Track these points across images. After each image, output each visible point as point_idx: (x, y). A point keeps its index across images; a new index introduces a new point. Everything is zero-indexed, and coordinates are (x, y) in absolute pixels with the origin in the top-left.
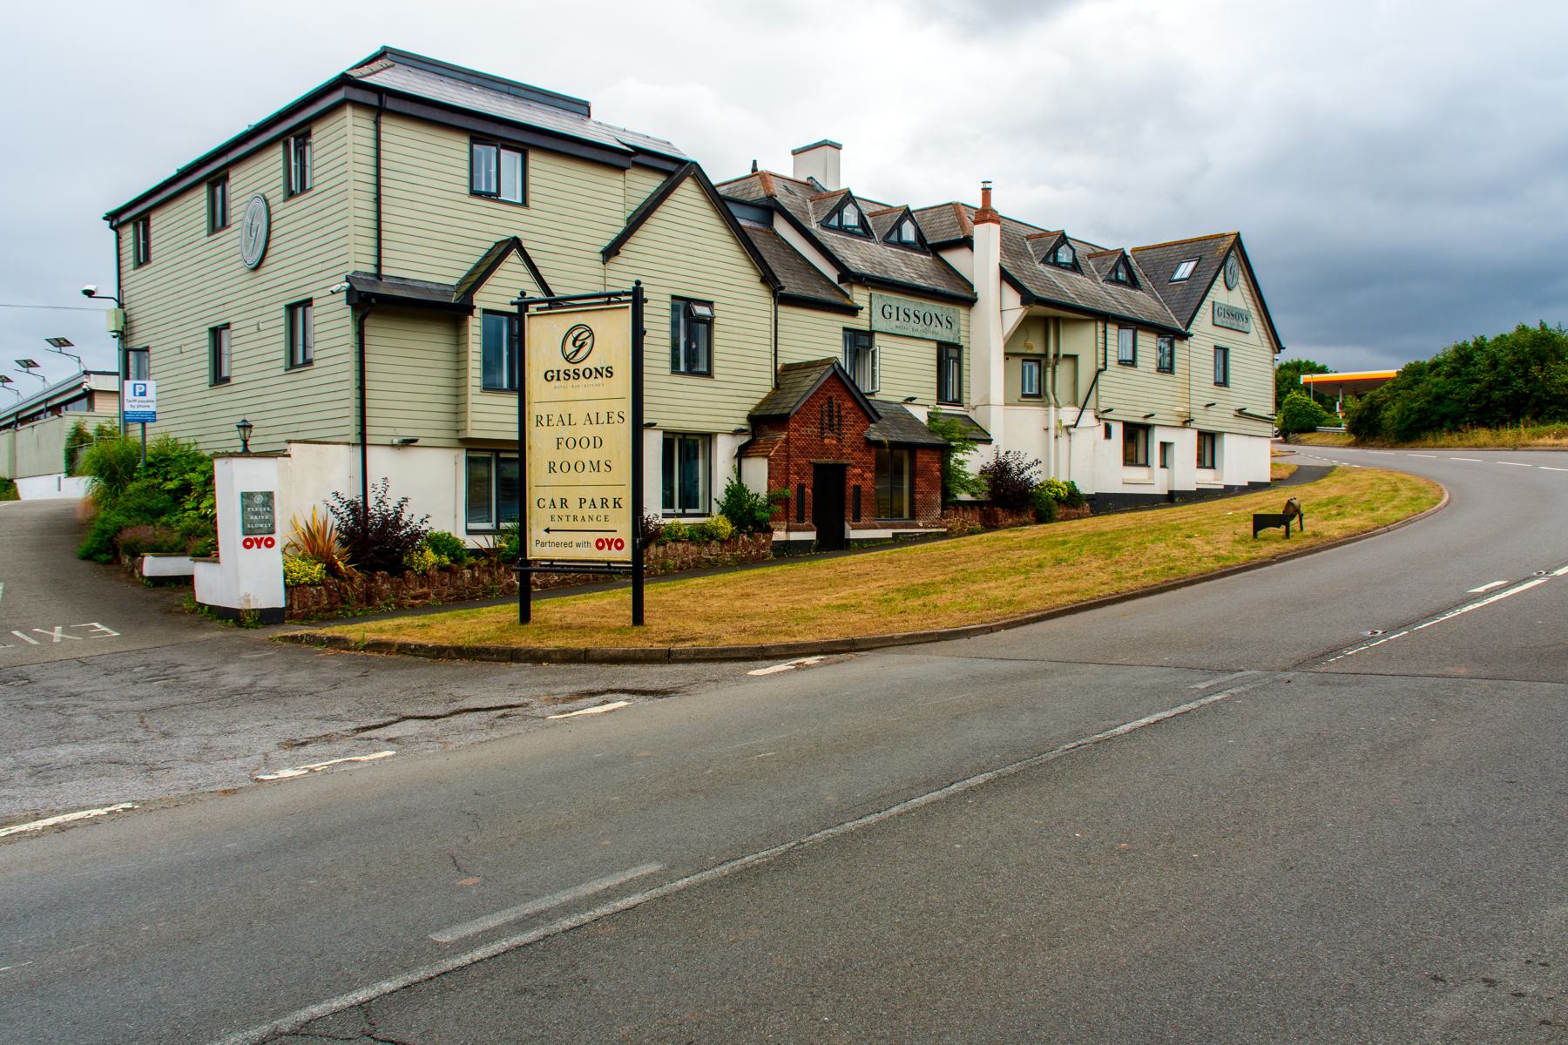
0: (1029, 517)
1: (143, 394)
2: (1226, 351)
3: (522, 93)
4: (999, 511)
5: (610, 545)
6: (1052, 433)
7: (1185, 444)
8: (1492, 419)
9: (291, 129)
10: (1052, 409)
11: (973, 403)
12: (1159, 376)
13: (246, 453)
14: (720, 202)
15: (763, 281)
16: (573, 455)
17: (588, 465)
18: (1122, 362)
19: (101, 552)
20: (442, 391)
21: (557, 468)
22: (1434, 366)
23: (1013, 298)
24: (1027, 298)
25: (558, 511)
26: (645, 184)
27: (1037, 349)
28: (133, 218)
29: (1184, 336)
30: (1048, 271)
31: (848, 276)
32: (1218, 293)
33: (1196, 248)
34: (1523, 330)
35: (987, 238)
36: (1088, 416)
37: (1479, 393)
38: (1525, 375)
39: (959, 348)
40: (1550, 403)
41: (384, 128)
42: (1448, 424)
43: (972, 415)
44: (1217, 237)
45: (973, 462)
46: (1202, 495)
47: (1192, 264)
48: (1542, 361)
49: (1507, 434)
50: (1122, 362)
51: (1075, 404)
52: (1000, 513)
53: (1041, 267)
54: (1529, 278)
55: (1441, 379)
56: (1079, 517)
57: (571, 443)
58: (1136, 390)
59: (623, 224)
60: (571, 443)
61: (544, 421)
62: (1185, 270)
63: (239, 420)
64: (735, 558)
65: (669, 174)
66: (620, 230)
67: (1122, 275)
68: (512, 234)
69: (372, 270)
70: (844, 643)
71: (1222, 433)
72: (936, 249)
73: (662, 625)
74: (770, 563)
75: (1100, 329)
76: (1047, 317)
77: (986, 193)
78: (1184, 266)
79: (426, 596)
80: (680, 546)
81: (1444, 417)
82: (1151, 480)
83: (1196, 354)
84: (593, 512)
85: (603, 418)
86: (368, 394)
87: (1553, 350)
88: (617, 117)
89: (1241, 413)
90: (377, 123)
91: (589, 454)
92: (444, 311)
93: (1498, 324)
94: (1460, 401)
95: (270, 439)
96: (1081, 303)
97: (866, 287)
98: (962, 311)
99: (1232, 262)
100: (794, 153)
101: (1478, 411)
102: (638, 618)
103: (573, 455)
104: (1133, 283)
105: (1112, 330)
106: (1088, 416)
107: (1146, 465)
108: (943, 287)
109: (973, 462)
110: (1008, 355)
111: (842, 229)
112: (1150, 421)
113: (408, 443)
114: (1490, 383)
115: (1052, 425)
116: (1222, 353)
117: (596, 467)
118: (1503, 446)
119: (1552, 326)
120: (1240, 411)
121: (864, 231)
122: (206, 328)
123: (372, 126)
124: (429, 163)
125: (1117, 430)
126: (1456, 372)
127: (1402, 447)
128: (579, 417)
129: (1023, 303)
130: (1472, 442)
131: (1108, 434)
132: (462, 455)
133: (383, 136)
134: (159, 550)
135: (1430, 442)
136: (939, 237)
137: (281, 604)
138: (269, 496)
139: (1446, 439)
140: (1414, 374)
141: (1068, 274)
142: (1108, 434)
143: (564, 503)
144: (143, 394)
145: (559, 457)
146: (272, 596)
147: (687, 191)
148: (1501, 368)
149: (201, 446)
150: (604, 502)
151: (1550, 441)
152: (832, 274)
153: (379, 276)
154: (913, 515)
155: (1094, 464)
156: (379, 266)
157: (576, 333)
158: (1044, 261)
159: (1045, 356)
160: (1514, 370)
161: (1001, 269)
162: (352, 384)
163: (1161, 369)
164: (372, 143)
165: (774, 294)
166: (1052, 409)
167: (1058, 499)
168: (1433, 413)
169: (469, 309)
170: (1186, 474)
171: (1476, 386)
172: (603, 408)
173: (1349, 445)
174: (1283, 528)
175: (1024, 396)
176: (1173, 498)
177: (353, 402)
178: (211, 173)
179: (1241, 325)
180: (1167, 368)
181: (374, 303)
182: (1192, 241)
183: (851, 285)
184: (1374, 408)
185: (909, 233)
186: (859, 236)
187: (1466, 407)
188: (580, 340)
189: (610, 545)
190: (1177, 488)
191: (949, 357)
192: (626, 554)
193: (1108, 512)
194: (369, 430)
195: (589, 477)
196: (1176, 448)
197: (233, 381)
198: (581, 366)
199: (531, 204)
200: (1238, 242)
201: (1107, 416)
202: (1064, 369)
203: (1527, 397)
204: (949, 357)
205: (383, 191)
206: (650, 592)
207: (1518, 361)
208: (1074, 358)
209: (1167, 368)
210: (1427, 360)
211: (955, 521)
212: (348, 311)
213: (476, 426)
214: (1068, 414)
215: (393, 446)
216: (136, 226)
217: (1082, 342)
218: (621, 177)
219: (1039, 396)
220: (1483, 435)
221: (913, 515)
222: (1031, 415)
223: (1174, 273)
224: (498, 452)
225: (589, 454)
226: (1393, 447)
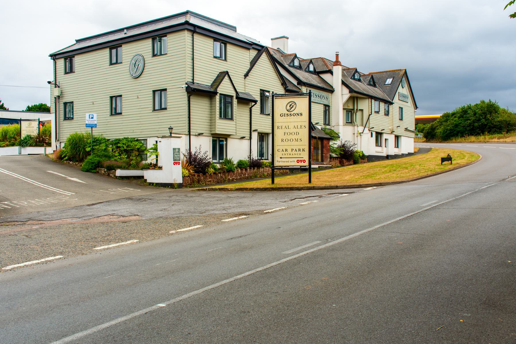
0: (352, 162)
1: (92, 118)
2: (402, 108)
3: (220, 24)
4: (344, 160)
5: (301, 161)
6: (356, 135)
7: (391, 139)
8: (474, 132)
9: (157, 33)
10: (356, 127)
11: (333, 125)
12: (385, 117)
13: (171, 136)
14: (273, 61)
15: (282, 84)
16: (291, 137)
17: (294, 140)
18: (376, 112)
19: (92, 169)
20: (207, 118)
21: (284, 140)
22: (453, 114)
23: (346, 91)
24: (351, 91)
25: (284, 152)
26: (253, 53)
27: (351, 107)
28: (66, 58)
29: (392, 103)
30: (353, 81)
31: (300, 83)
32: (400, 90)
33: (392, 74)
34: (483, 102)
35: (337, 71)
36: (366, 130)
37: (470, 123)
38: (485, 118)
39: (329, 106)
40: (493, 128)
41: (195, 37)
42: (459, 134)
43: (332, 129)
44: (399, 70)
45: (335, 144)
46: (396, 157)
47: (391, 79)
48: (491, 113)
49: (482, 138)
50: (376, 112)
51: (362, 125)
52: (345, 161)
53: (351, 80)
54: (469, 81)
55: (457, 119)
56: (364, 163)
57: (289, 134)
58: (379, 122)
59: (249, 66)
60: (289, 134)
61: (280, 128)
62: (389, 81)
63: (169, 126)
64: (281, 173)
65: (259, 50)
66: (248, 68)
67: (372, 83)
68: (225, 70)
69: (191, 81)
70: (379, 184)
71: (401, 136)
72: (317, 73)
73: (315, 182)
74: (289, 175)
75: (370, 101)
76: (356, 96)
77: (337, 56)
78: (388, 80)
79: (210, 181)
80: (267, 168)
81: (458, 132)
82: (382, 151)
83: (394, 110)
84: (296, 153)
85: (299, 127)
86: (191, 119)
87: (494, 109)
88: (244, 33)
89: (406, 129)
90: (193, 35)
91: (294, 137)
92: (209, 94)
93: (473, 99)
94: (464, 126)
95: (143, 133)
96: (365, 92)
97: (306, 86)
98: (330, 94)
99: (404, 79)
100: (272, 39)
101: (470, 130)
102: (310, 181)
103: (291, 137)
104: (374, 85)
105: (373, 101)
106: (366, 130)
107: (381, 146)
108: (325, 87)
109: (335, 144)
110: (344, 109)
111: (294, 66)
112: (383, 132)
113: (200, 134)
114: (474, 120)
115: (356, 132)
116: (401, 109)
117: (297, 140)
118: (480, 142)
119: (493, 101)
120: (406, 129)
121: (300, 68)
122: (109, 96)
123: (191, 36)
124: (205, 46)
125: (374, 134)
126: (461, 116)
127: (444, 143)
128: (291, 126)
129: (350, 92)
130: (469, 141)
131: (372, 136)
132: (211, 138)
133: (195, 40)
134: (121, 168)
135: (454, 141)
136: (322, 68)
137: (182, 182)
138: (179, 149)
139: (460, 140)
140: (446, 117)
141: (358, 82)
142: (372, 136)
143: (286, 150)
144: (92, 118)
145: (284, 138)
146: (180, 181)
147: (264, 56)
148: (477, 115)
149: (104, 136)
150: (299, 150)
151: (496, 140)
152: (295, 82)
153: (193, 83)
154: (322, 161)
155: (366, 146)
156: (193, 80)
157: (290, 104)
158: (351, 78)
159: (353, 109)
160: (482, 116)
161: (342, 81)
162: (187, 116)
163: (385, 115)
164: (191, 42)
165: (285, 89)
166: (356, 127)
167: (359, 156)
168: (455, 131)
169: (216, 93)
170: (392, 150)
171: (469, 121)
172: (299, 124)
173: (424, 142)
174: (450, 161)
175: (347, 123)
176: (388, 157)
177: (187, 122)
178: (112, 44)
179: (406, 100)
180: (387, 114)
181: (193, 91)
182: (390, 71)
183: (302, 85)
184: (433, 129)
185: (311, 68)
186: (298, 69)
187: (466, 129)
188: (292, 105)
189: (301, 161)
190: (389, 154)
191: (327, 108)
192: (307, 164)
193: (373, 161)
194: (191, 130)
195: (294, 143)
196: (389, 140)
197: (123, 114)
198: (292, 113)
199: (228, 60)
200: (406, 72)
201: (372, 130)
202: (359, 114)
203: (486, 125)
204: (327, 108)
205: (195, 57)
206: (313, 174)
207: (483, 113)
208: (362, 110)
209: (387, 114)
210: (450, 112)
211: (333, 163)
212: (186, 93)
213: (218, 129)
214: (361, 129)
215: (196, 135)
216: (66, 59)
217: (364, 105)
218: (248, 51)
219: (351, 123)
220: (473, 138)
221: (322, 161)
222: (349, 129)
223: (385, 82)
224: (219, 138)
225: (294, 137)
226: (440, 142)
